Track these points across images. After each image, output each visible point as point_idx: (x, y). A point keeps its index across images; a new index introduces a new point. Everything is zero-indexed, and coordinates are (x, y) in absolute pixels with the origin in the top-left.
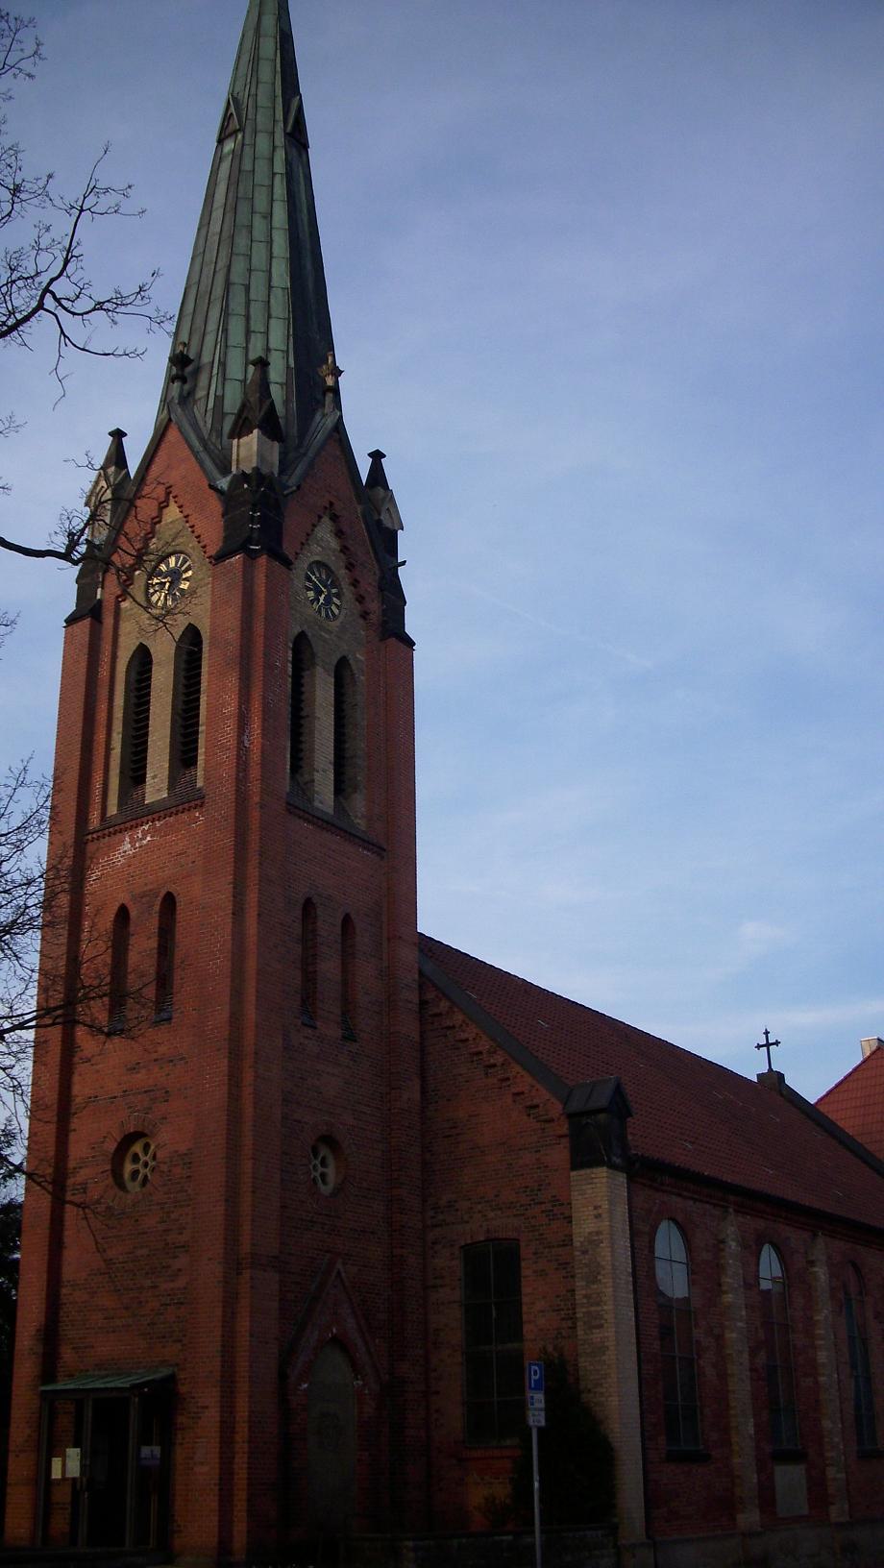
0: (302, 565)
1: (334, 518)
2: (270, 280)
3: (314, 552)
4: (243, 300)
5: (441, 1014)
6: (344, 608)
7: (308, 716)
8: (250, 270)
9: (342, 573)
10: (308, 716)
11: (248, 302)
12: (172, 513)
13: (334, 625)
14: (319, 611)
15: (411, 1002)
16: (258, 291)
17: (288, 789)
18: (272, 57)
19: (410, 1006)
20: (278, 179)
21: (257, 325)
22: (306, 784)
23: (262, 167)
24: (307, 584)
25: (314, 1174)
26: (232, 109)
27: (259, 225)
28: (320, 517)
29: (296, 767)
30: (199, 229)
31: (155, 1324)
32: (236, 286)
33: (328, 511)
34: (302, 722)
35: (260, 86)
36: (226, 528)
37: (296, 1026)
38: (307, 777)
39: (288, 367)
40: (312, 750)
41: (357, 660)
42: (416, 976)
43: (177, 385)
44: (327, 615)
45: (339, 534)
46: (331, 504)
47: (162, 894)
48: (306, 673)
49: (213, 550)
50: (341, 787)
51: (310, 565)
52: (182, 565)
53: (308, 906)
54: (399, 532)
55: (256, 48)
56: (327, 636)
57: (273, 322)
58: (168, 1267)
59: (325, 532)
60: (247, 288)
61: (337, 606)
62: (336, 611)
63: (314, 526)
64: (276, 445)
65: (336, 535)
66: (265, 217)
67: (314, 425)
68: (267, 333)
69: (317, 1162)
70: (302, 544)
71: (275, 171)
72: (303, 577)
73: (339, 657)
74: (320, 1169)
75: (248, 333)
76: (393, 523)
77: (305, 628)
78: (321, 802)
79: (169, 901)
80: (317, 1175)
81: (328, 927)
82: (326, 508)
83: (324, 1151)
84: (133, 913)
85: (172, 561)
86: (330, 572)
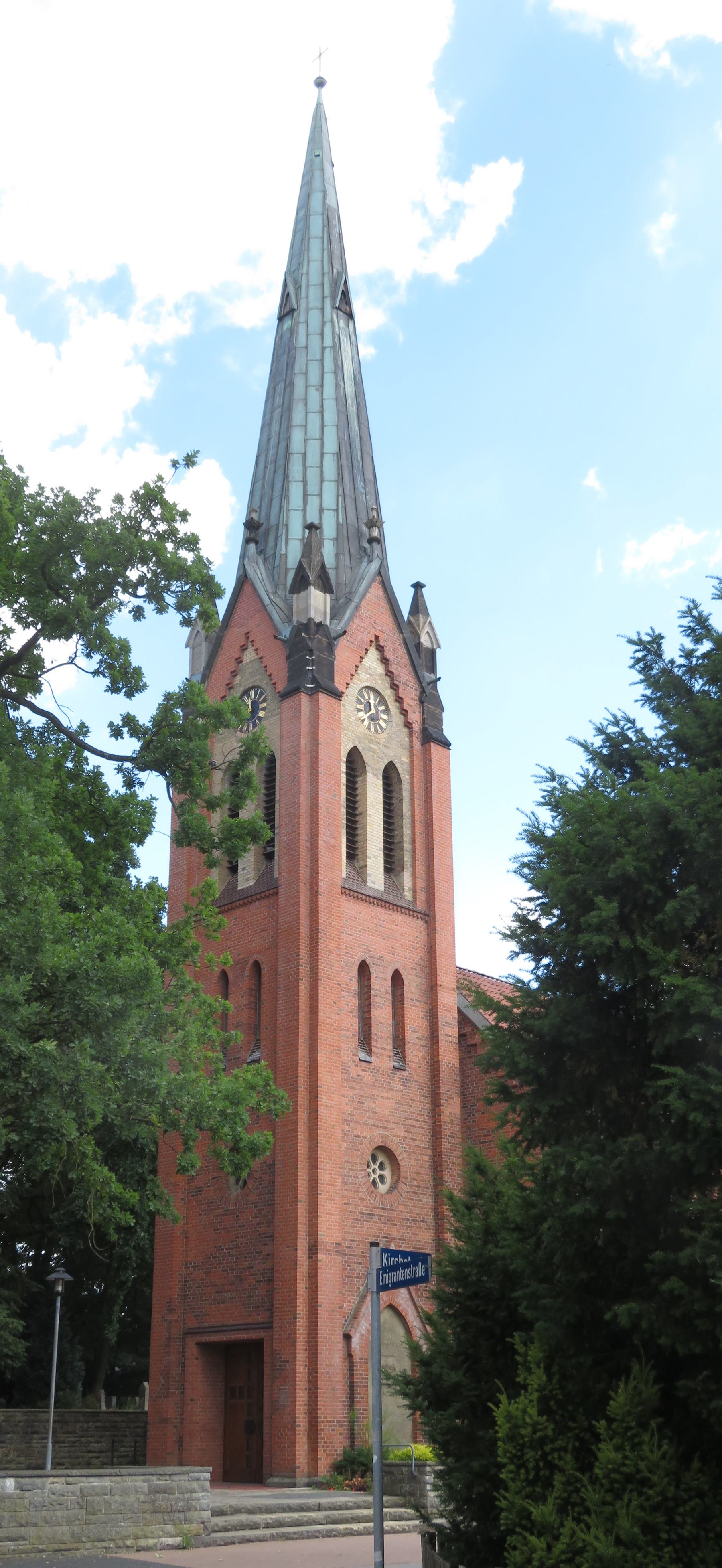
0: (351, 695)
1: (380, 649)
2: (322, 472)
3: (363, 679)
4: (301, 468)
5: (475, 1045)
6: (390, 722)
7: (361, 814)
8: (307, 413)
9: (388, 693)
10: (361, 814)
11: (305, 468)
12: (249, 656)
13: (383, 737)
14: (369, 728)
15: (450, 1036)
16: (313, 459)
17: (344, 875)
18: (320, 234)
19: (450, 1039)
20: (327, 351)
21: (313, 488)
22: (361, 868)
23: (315, 341)
24: (359, 706)
25: (373, 1176)
26: (291, 289)
27: (314, 395)
28: (367, 650)
29: (352, 856)
30: (266, 402)
31: (252, 1297)
32: (296, 455)
33: (374, 644)
34: (357, 819)
35: (311, 263)
36: (290, 670)
37: (354, 1062)
38: (361, 863)
39: (338, 524)
40: (365, 842)
41: (402, 763)
42: (456, 1015)
43: (252, 546)
44: (376, 730)
45: (384, 661)
46: (377, 637)
47: (250, 963)
48: (359, 779)
49: (281, 687)
50: (392, 866)
51: (361, 690)
52: (259, 697)
53: (364, 969)
54: (438, 651)
55: (307, 227)
56: (376, 748)
57: (325, 484)
58: (261, 1252)
59: (372, 659)
60: (304, 456)
61: (385, 721)
62: (383, 725)
63: (362, 658)
64: (328, 596)
65: (382, 662)
66: (317, 390)
67: (361, 571)
68: (320, 495)
69: (376, 1167)
70: (352, 675)
71: (325, 345)
72: (354, 700)
73: (386, 762)
74: (379, 1172)
75: (305, 496)
76: (432, 643)
77: (357, 744)
78: (373, 883)
79: (257, 966)
80: (376, 1176)
81: (381, 984)
82: (371, 642)
83: (381, 1158)
84: (231, 976)
85: (252, 693)
86: (377, 693)
